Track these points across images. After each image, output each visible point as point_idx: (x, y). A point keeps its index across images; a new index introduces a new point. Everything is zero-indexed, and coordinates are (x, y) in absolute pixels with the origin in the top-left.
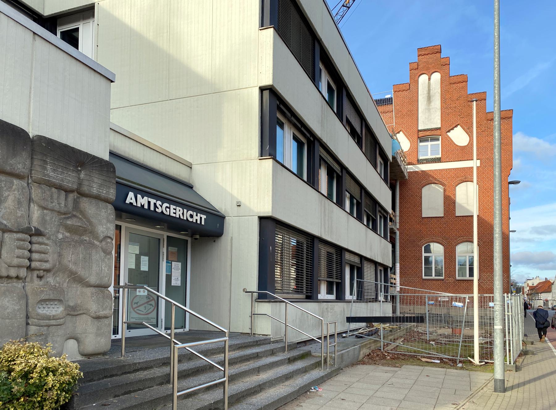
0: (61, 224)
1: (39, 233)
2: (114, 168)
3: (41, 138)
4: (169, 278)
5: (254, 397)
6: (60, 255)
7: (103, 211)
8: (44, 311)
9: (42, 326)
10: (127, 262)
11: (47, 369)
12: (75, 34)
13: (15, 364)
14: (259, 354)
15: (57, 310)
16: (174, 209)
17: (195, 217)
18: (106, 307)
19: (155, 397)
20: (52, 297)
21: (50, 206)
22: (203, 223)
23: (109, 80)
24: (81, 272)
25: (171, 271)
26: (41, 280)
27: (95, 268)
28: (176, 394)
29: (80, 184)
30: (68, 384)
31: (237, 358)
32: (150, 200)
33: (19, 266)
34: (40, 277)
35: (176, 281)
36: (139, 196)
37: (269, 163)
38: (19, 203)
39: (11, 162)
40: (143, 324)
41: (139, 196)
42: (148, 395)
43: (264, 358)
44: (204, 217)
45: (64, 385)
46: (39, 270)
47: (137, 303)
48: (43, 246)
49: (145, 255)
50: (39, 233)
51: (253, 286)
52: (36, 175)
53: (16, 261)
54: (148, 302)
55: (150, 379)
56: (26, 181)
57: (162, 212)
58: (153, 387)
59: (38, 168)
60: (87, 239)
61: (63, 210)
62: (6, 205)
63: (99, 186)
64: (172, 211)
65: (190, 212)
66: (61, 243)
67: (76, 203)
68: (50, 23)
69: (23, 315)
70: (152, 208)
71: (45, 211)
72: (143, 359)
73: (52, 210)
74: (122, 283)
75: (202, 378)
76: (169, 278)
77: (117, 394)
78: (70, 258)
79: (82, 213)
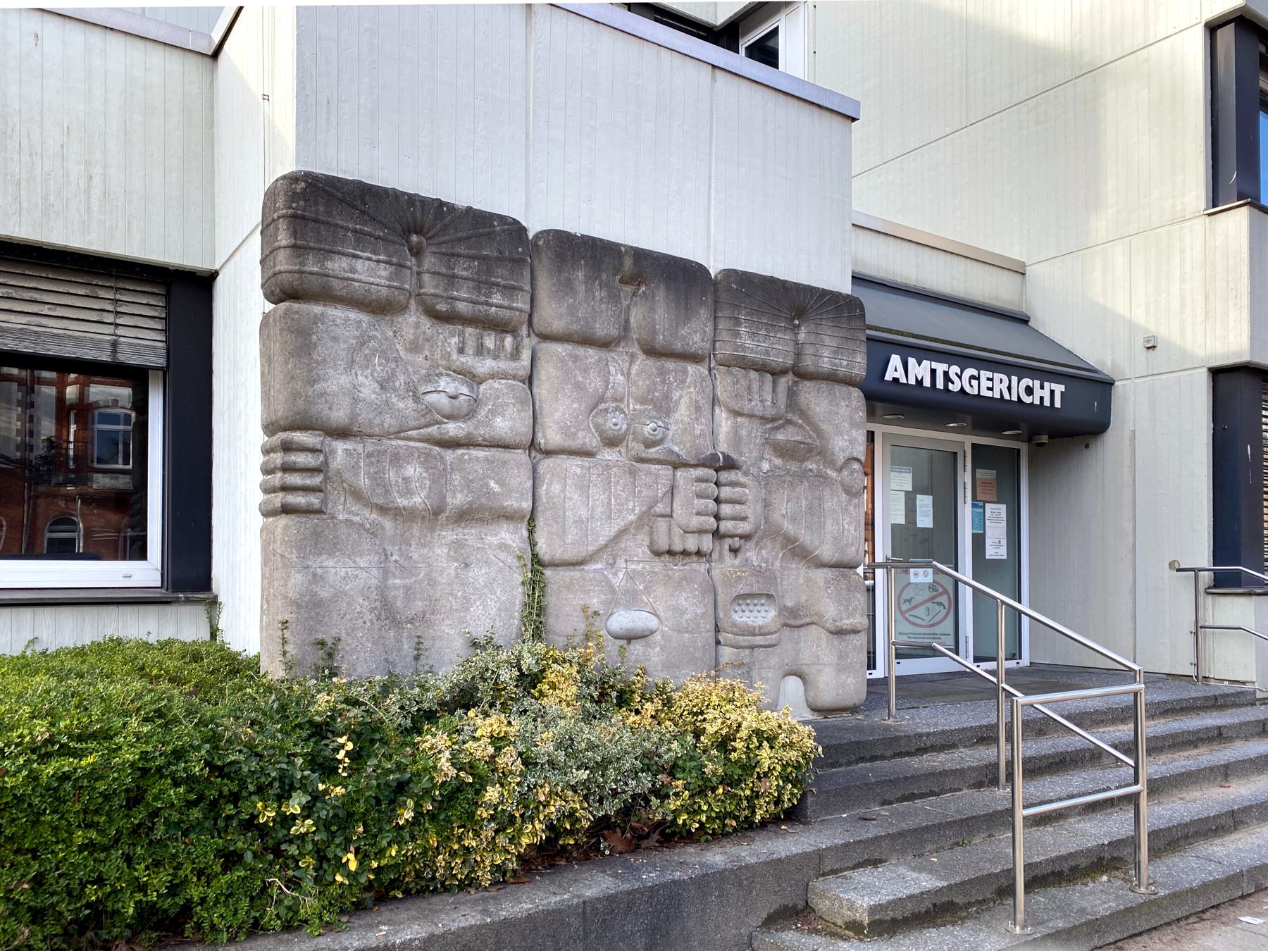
0: (767, 442)
1: (730, 465)
2: (862, 309)
3: (729, 274)
4: (979, 542)
5: (1218, 841)
6: (767, 504)
9: (741, 647)
10: (889, 512)
11: (758, 733)
13: (705, 720)
14: (1224, 731)
15: (763, 616)
16: (988, 379)
17: (1038, 393)
18: (855, 610)
19: (968, 814)
20: (755, 589)
21: (747, 407)
22: (1058, 404)
23: (848, 117)
24: (806, 537)
25: (984, 524)
26: (736, 556)
27: (830, 526)
28: (1021, 813)
29: (798, 355)
30: (795, 768)
31: (1163, 738)
32: (935, 365)
33: (701, 532)
34: (735, 551)
35: (996, 549)
36: (912, 361)
37: (1238, 220)
38: (698, 409)
40: (934, 649)
41: (912, 361)
42: (953, 807)
43: (1238, 744)
44: (1059, 388)
45: (789, 769)
46: (732, 536)
47: (909, 601)
48: (738, 489)
49: (925, 492)
50: (730, 465)
51: (1200, 553)
52: (724, 351)
53: (696, 522)
54: (933, 598)
55: (954, 772)
56: (706, 366)
57: (962, 388)
58: (960, 790)
59: (725, 336)
60: (814, 466)
61: (770, 412)
62: (677, 416)
64: (985, 384)
65: (1027, 381)
66: (766, 481)
67: (792, 394)
68: (726, 36)
69: (710, 626)
70: (940, 385)
72: (936, 725)
73: (751, 416)
74: (879, 558)
75: (1076, 780)
76: (979, 542)
77: (887, 797)
78: (785, 508)
79: (803, 414)
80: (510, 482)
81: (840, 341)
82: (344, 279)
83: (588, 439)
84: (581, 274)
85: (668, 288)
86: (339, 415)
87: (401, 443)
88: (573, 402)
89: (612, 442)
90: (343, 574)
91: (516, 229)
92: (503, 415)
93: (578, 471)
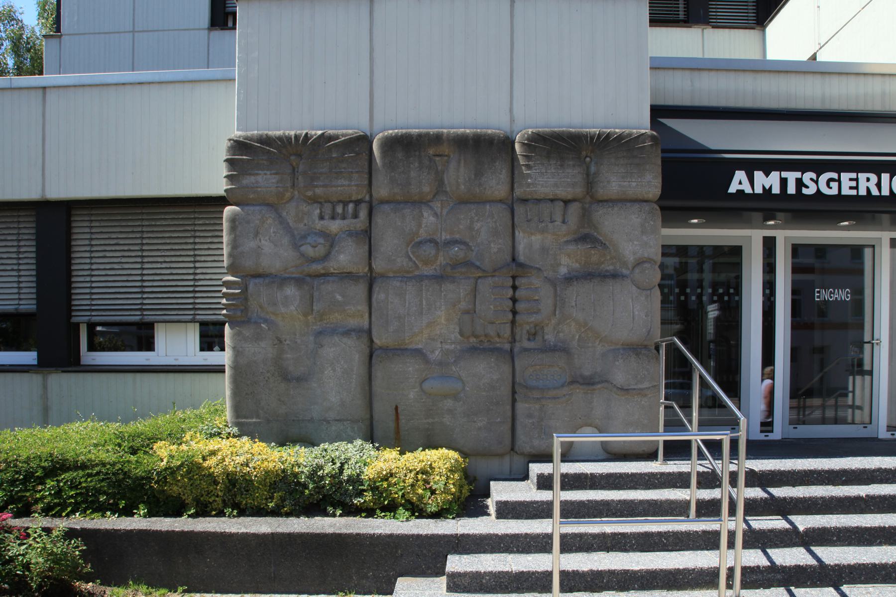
12: (217, 348)
32: (784, 174)
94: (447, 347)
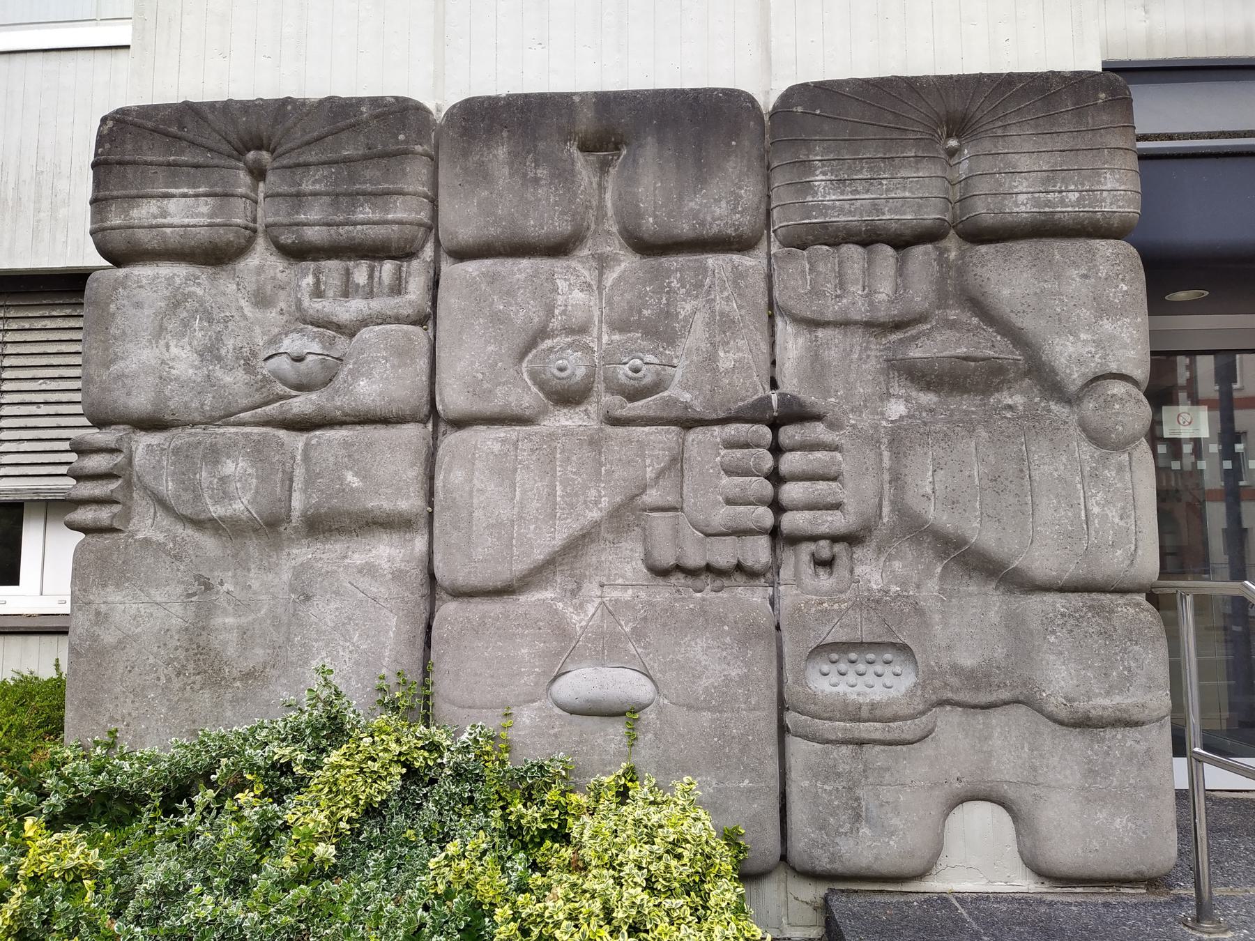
1: (796, 413)
7: (1074, 273)
8: (828, 683)
9: (828, 742)
15: (884, 684)
21: (832, 309)
27: (1050, 511)
39: (692, 204)
46: (814, 538)
48: (818, 455)
50: (796, 413)
53: (722, 516)
63: (1044, 182)
66: (899, 439)
71: (820, 333)
73: (844, 324)
80: (384, 469)
81: (1058, 157)
82: (151, 227)
83: (526, 397)
84: (502, 152)
85: (661, 142)
86: (140, 401)
87: (233, 430)
88: (488, 342)
89: (568, 397)
90: (133, 612)
91: (401, 113)
92: (369, 375)
93: (497, 448)
94: (616, 594)
